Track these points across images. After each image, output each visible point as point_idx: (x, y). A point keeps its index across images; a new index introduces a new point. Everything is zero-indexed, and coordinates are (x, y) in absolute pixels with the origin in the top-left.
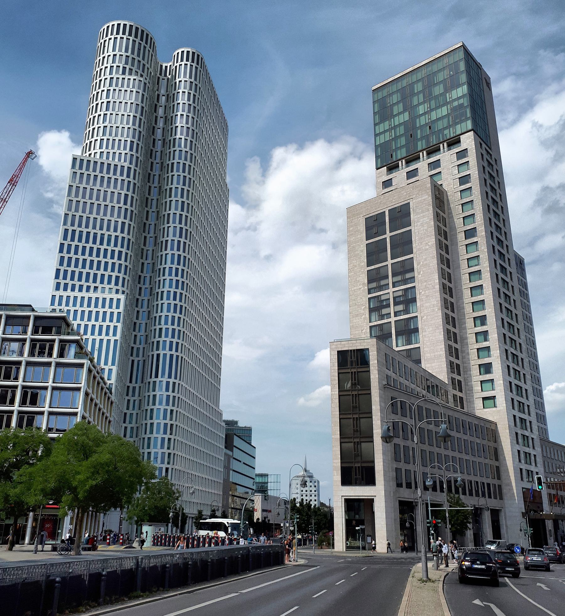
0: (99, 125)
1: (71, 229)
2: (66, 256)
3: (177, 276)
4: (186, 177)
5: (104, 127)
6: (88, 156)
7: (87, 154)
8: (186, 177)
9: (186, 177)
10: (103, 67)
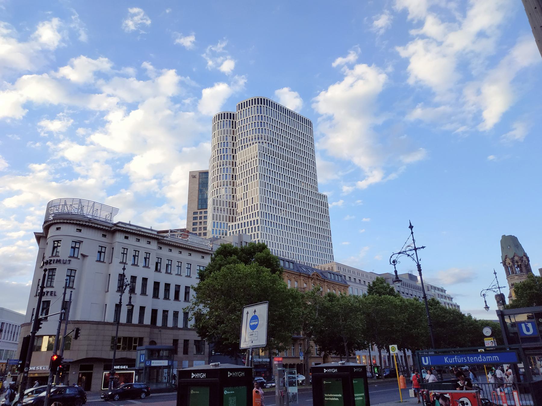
2: (216, 207)
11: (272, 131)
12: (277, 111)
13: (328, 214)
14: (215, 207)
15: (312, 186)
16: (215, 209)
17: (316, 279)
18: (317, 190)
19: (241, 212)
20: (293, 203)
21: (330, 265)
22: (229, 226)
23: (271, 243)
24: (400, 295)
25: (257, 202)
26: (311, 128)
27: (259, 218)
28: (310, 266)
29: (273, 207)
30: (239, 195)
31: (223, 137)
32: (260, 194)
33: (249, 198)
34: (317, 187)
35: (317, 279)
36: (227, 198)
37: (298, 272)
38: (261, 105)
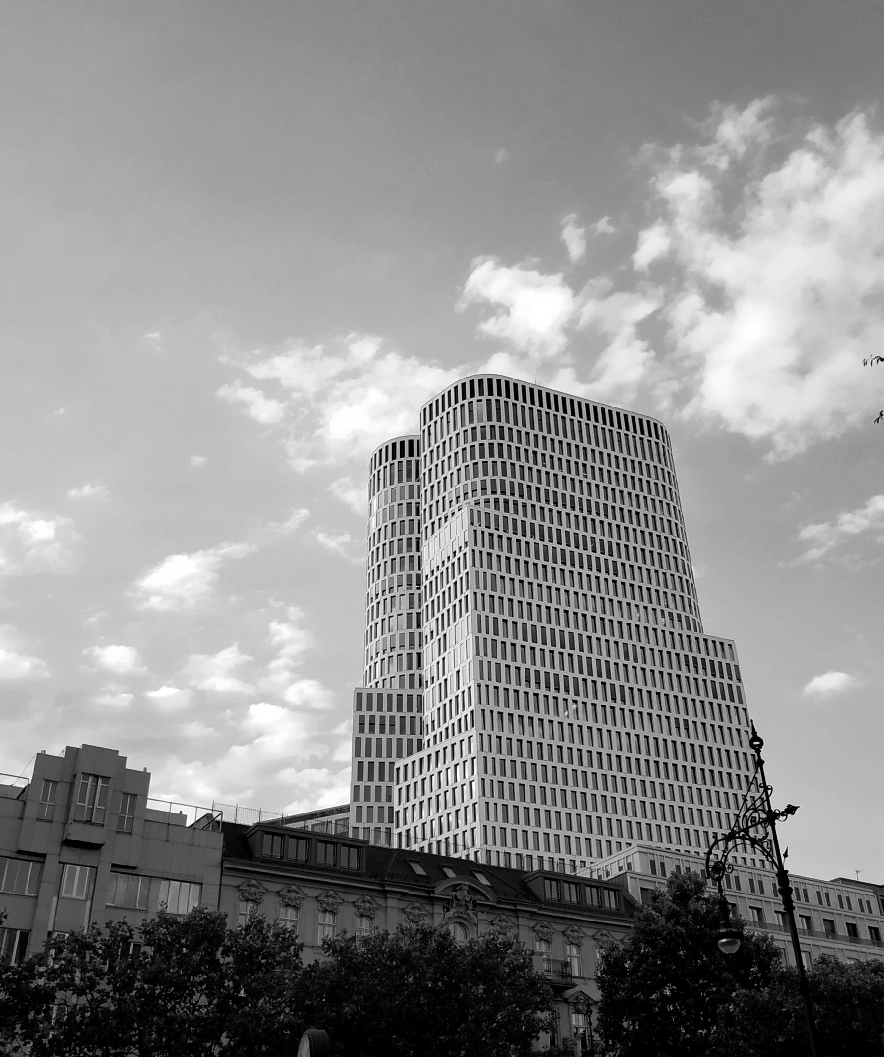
0: (385, 560)
1: (366, 761)
2: (367, 715)
3: (491, 420)
4: (505, 463)
5: (392, 597)
6: (374, 687)
7: (373, 683)
8: (505, 463)
9: (505, 463)
10: (380, 545)
11: (617, 490)
12: (646, 437)
13: (741, 701)
14: (362, 718)
15: (671, 614)
16: (362, 724)
17: (470, 905)
18: (698, 628)
19: (433, 722)
20: (724, 698)
21: (621, 857)
22: (398, 769)
23: (682, 832)
24: (776, 944)
25: (469, 681)
26: (666, 445)
27: (473, 732)
28: (443, 854)
29: (730, 729)
30: (429, 668)
31: (392, 508)
32: (478, 654)
33: (451, 674)
34: (697, 620)
35: (475, 905)
36: (402, 685)
37: (372, 880)
38: (499, 398)
